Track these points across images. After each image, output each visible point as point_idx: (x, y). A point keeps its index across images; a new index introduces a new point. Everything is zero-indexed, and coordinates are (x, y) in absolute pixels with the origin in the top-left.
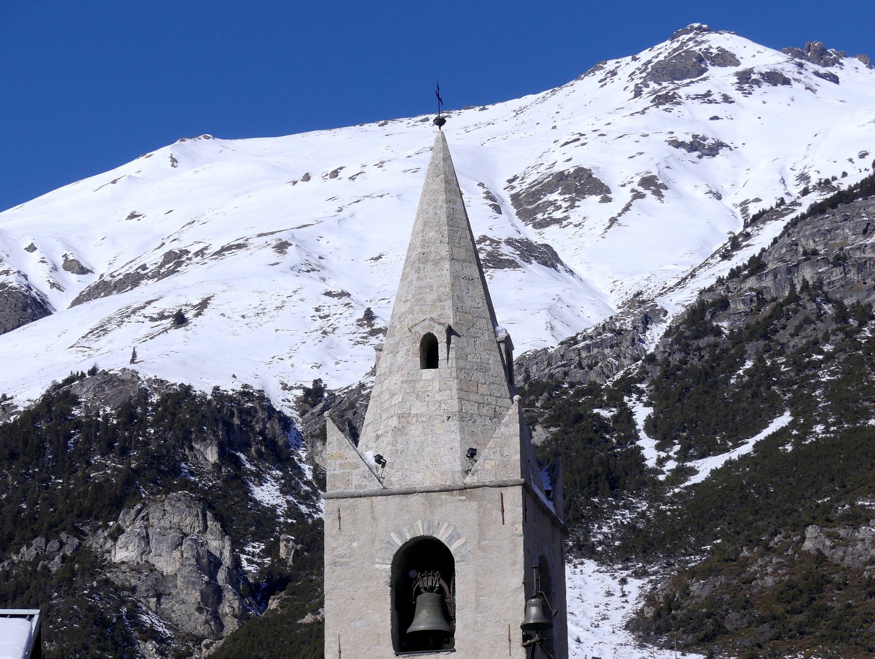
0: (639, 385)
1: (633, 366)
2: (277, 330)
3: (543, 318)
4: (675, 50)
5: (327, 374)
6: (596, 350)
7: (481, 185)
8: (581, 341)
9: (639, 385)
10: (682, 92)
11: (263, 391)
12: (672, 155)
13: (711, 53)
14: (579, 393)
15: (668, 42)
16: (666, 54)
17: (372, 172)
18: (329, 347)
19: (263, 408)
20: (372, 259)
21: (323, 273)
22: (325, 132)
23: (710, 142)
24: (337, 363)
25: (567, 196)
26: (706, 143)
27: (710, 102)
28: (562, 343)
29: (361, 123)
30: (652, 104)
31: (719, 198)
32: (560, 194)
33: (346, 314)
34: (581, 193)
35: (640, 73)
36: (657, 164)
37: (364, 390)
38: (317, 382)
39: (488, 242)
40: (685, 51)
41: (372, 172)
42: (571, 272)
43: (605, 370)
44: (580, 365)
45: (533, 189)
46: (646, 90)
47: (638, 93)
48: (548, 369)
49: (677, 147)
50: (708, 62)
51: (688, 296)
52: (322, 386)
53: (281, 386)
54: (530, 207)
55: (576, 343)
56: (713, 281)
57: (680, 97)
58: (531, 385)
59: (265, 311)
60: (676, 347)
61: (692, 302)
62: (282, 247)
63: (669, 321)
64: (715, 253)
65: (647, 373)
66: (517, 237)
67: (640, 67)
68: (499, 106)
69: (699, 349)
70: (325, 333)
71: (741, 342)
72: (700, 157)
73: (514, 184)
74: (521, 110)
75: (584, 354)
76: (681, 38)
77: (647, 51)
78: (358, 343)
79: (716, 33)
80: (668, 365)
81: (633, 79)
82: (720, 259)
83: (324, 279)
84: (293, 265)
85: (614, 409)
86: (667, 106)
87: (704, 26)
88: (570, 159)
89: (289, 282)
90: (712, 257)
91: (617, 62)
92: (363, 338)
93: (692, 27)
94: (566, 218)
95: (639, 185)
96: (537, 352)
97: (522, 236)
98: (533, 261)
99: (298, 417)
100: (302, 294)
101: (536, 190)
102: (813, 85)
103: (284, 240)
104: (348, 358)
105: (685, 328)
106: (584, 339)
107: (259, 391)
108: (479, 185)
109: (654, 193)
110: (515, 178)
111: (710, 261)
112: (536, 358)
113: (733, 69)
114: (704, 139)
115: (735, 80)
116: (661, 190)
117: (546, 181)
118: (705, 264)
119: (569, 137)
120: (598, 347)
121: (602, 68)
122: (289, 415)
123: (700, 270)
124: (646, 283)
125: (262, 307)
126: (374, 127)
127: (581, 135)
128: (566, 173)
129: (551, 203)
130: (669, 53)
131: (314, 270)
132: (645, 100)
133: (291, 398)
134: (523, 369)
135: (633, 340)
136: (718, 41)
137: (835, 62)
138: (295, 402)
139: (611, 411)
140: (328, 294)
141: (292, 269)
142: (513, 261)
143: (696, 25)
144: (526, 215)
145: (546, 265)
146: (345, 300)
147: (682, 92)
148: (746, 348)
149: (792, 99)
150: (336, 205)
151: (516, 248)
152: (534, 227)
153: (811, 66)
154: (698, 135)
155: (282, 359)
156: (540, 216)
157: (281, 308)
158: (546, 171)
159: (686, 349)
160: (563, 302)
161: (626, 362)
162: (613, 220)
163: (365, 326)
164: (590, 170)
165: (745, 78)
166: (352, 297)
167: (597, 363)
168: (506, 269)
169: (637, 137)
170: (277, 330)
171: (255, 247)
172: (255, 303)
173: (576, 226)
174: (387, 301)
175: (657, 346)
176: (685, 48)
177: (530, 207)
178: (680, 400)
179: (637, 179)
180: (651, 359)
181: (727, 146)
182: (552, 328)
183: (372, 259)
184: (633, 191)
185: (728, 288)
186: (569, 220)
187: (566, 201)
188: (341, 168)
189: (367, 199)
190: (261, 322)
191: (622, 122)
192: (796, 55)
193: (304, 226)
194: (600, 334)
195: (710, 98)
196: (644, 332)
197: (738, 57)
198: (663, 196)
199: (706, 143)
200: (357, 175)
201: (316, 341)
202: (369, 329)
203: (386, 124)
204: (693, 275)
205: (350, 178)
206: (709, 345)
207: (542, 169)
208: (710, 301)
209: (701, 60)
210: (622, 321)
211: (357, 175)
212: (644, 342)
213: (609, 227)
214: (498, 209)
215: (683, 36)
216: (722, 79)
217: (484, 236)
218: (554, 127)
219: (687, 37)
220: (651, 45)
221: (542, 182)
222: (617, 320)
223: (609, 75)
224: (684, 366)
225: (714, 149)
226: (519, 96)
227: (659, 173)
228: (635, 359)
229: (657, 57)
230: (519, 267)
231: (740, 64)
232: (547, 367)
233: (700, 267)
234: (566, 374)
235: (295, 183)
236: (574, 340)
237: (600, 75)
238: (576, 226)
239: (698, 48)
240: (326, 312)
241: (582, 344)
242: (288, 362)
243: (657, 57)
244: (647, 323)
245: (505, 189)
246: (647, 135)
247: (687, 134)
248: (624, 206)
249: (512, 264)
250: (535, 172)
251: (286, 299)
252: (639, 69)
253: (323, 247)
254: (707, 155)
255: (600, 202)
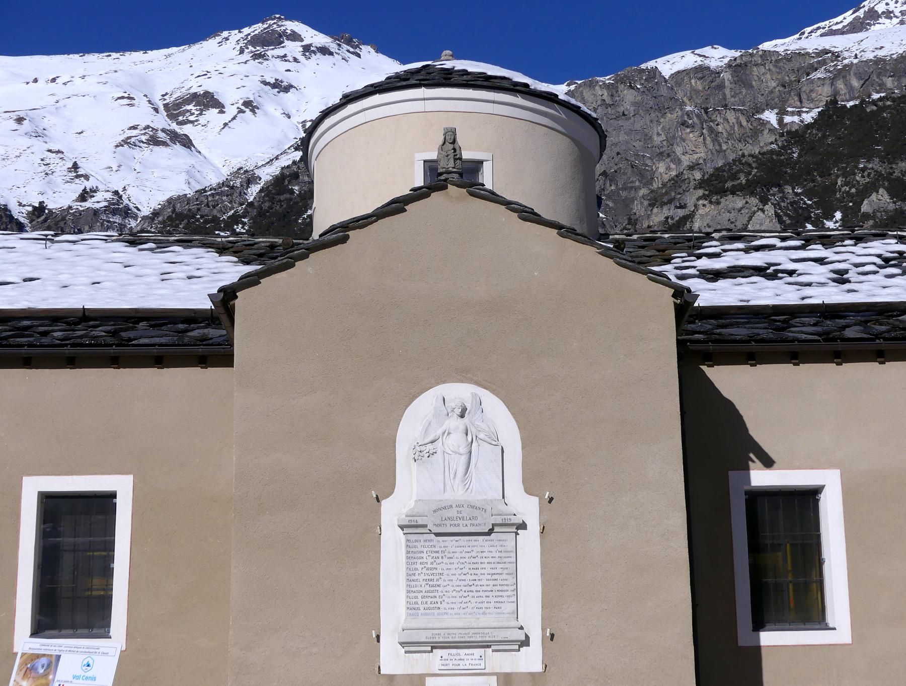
0: (243, 220)
1: (240, 208)
2: (16, 170)
3: (183, 177)
4: (265, 29)
5: (48, 199)
6: (217, 197)
7: (145, 96)
8: (209, 191)
9: (243, 220)
10: (270, 53)
11: (7, 205)
12: (262, 89)
13: (287, 33)
14: (207, 222)
15: (260, 24)
16: (260, 31)
17: (78, 81)
18: (49, 183)
19: (7, 216)
20: (77, 133)
21: (45, 139)
22: (45, 56)
23: (285, 84)
24: (54, 193)
25: (198, 108)
26: (283, 84)
27: (286, 61)
28: (196, 192)
29: (68, 52)
30: (251, 58)
31: (289, 117)
32: (194, 106)
33: (61, 164)
34: (207, 106)
35: (243, 40)
36: (253, 94)
37: (72, 210)
38: (41, 203)
39: (150, 129)
40: (271, 30)
41: (78, 81)
42: (200, 152)
43: (223, 209)
44: (207, 205)
45: (177, 102)
46: (246, 51)
47: (242, 52)
48: (188, 206)
49: (266, 85)
50: (285, 38)
51: (274, 170)
52: (45, 206)
53: (18, 204)
54: (175, 112)
55: (206, 191)
56: (290, 162)
57: (268, 56)
58: (177, 214)
59: (8, 158)
60: (267, 199)
61: (276, 174)
62: (20, 120)
63: (262, 184)
64: (291, 146)
65: (248, 213)
66: (168, 128)
67: (243, 37)
68: (155, 52)
69: (280, 201)
70: (47, 174)
71: (306, 199)
72: (278, 92)
73: (165, 97)
74: (170, 55)
75: (210, 199)
76: (269, 22)
77: (247, 28)
78: (68, 182)
79: (291, 21)
80: (261, 209)
81: (238, 44)
82: (294, 150)
83: (46, 142)
84: (27, 132)
85: (228, 232)
86: (260, 60)
87: (282, 17)
88: (201, 86)
89: (26, 142)
90: (289, 148)
91: (229, 33)
92: (71, 179)
93: (275, 17)
94: (197, 121)
95: (242, 105)
96: (179, 196)
97: (171, 128)
98: (177, 143)
99: (28, 223)
100: (33, 149)
101: (179, 102)
102: (347, 57)
103: (21, 116)
104: (61, 190)
105: (271, 188)
106: (211, 190)
107: (4, 205)
108: (144, 96)
109: (251, 110)
110: (166, 94)
111: (288, 151)
112: (179, 199)
113: (300, 44)
114: (282, 82)
115: (301, 49)
116: (255, 109)
117: (185, 97)
118: (285, 152)
119: (200, 73)
120: (219, 195)
121: (220, 35)
122: (22, 222)
123: (282, 156)
124: (245, 162)
125: (6, 155)
126: (76, 57)
127: (208, 72)
128: (198, 94)
129: (188, 111)
130: (261, 30)
131: (40, 136)
132: (247, 56)
133: (24, 211)
134: (171, 205)
135: (241, 193)
136: (291, 26)
137: (357, 47)
138: (27, 214)
139: (226, 233)
140: (50, 151)
141: (26, 134)
142: (166, 142)
143: (278, 16)
144: (172, 116)
145: (185, 147)
146: (60, 155)
147: (270, 53)
148: (308, 203)
149: (334, 64)
150: (55, 99)
151: (167, 134)
152: (177, 124)
153: (345, 47)
154: (278, 79)
155: (19, 188)
156: (181, 118)
157: (19, 157)
158: (186, 92)
159: (272, 200)
160: (195, 168)
161: (235, 205)
162: (226, 125)
163: (73, 172)
164: (213, 93)
165: (307, 49)
166: (64, 154)
167: (218, 205)
168: (161, 146)
169: (242, 77)
170: (16, 170)
171: (3, 119)
172: (3, 152)
173: (202, 126)
174: (86, 159)
175: (255, 198)
176: (271, 28)
177: (175, 112)
178: (268, 230)
179: (241, 102)
180: (251, 204)
181: (295, 87)
182: (189, 183)
183: (77, 133)
184: (238, 108)
185: (299, 167)
186: (199, 122)
187: (197, 111)
188: (58, 77)
189: (74, 97)
190: (6, 165)
191: (232, 67)
192: (336, 39)
193: (34, 109)
194: (220, 188)
195: (286, 59)
196: (247, 189)
197: (302, 37)
198: (256, 113)
199: (283, 84)
200: (68, 82)
201: (41, 179)
202: (75, 174)
203: (84, 55)
204: (277, 158)
205: (64, 84)
206: (286, 199)
207: (183, 90)
208: (288, 173)
209: (280, 36)
210: (234, 181)
211: (68, 82)
212: (247, 195)
213: (223, 128)
214: (156, 110)
215: (270, 21)
216: (294, 48)
217: (148, 126)
218: (191, 66)
219: (273, 22)
220: (250, 25)
221: (183, 97)
222: (231, 180)
223: (224, 40)
224: (271, 211)
225: (287, 89)
226: (168, 48)
227: (254, 99)
228: (241, 204)
229: (254, 32)
230: (169, 146)
231: (304, 41)
232: (187, 205)
233: (281, 154)
234: (199, 209)
235: (28, 83)
236: (204, 190)
237: (218, 39)
238: (202, 126)
239: (279, 29)
240: (48, 162)
241: (209, 193)
242: (23, 190)
243: (254, 32)
244: (249, 184)
245: (160, 100)
246: (248, 76)
247: (272, 78)
248: (232, 117)
249: (164, 144)
250: (179, 91)
251: (22, 152)
252: (242, 38)
253: (46, 123)
254: (283, 92)
255: (218, 113)
